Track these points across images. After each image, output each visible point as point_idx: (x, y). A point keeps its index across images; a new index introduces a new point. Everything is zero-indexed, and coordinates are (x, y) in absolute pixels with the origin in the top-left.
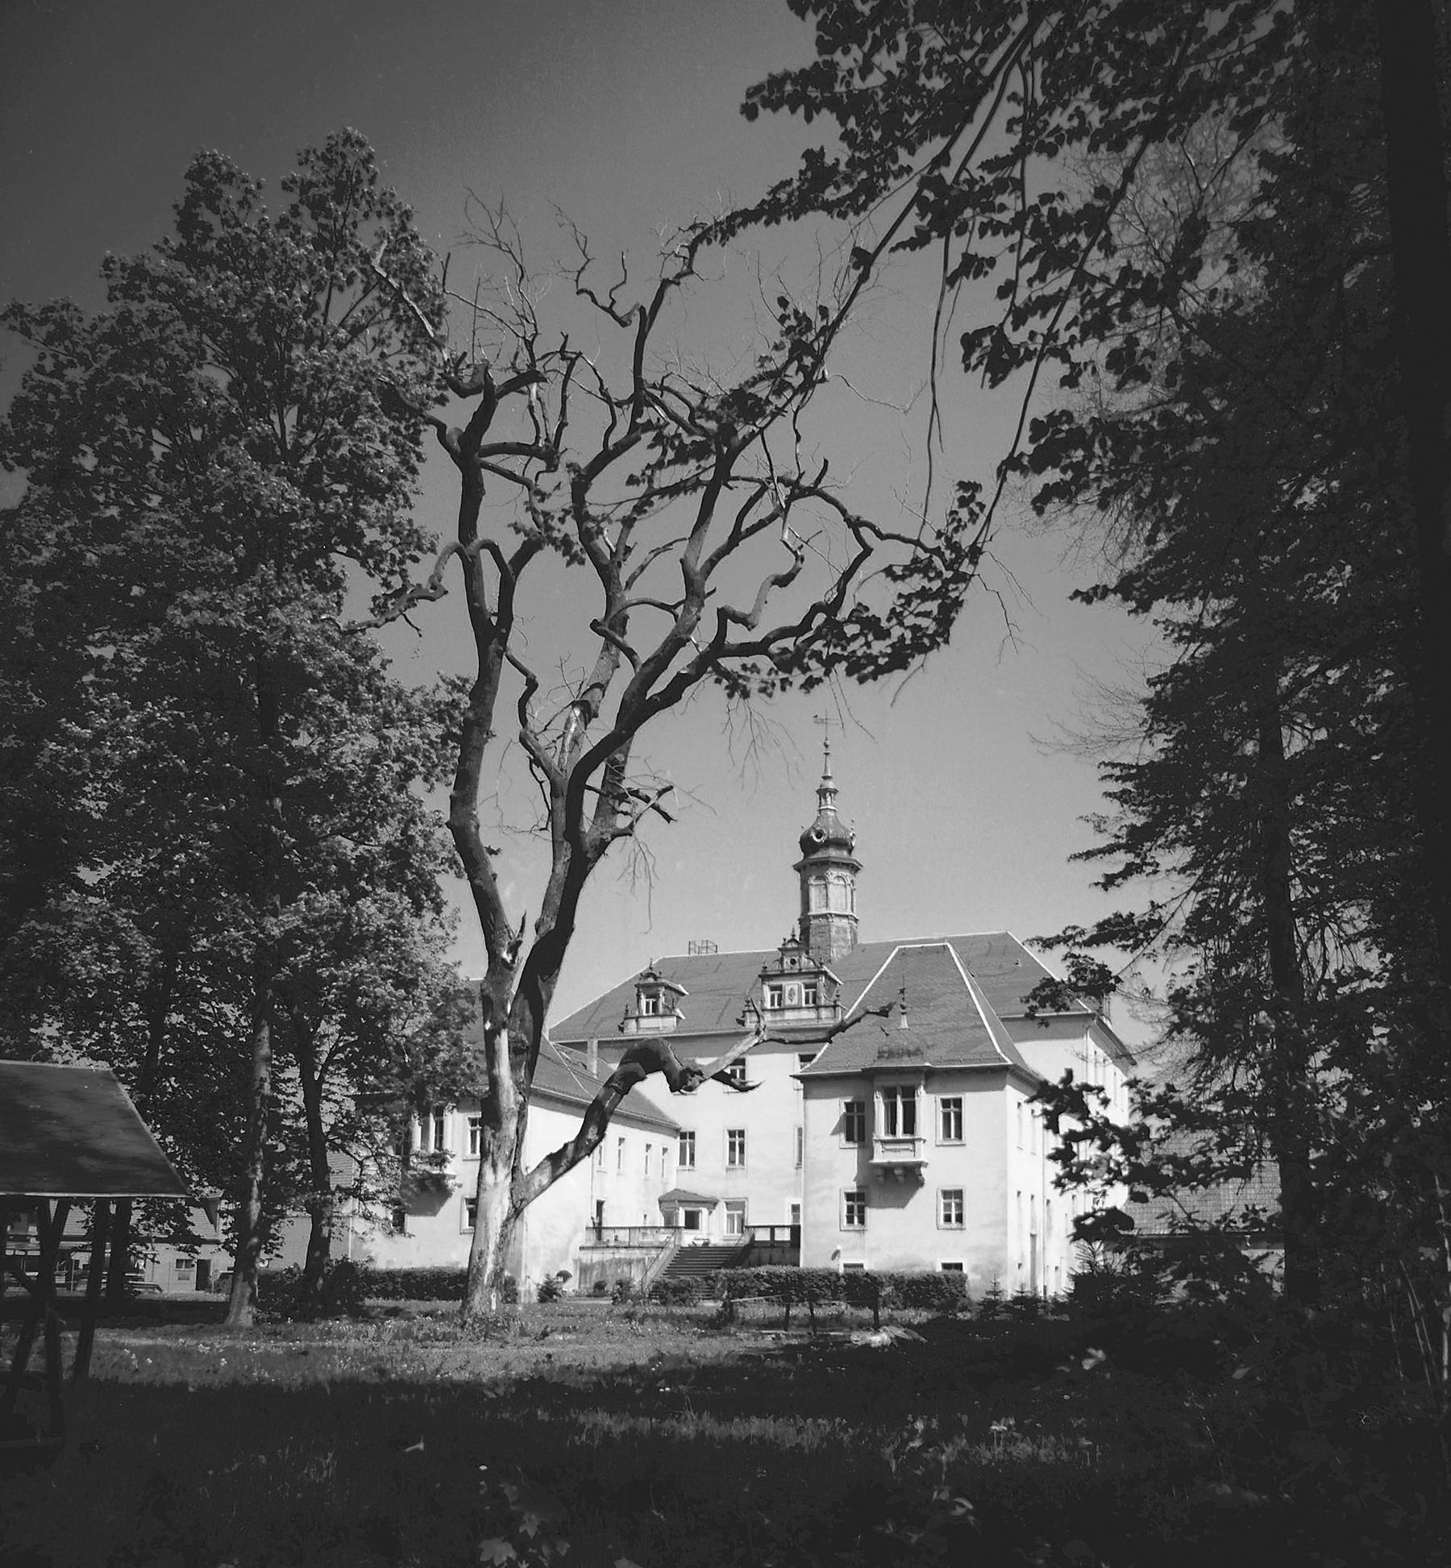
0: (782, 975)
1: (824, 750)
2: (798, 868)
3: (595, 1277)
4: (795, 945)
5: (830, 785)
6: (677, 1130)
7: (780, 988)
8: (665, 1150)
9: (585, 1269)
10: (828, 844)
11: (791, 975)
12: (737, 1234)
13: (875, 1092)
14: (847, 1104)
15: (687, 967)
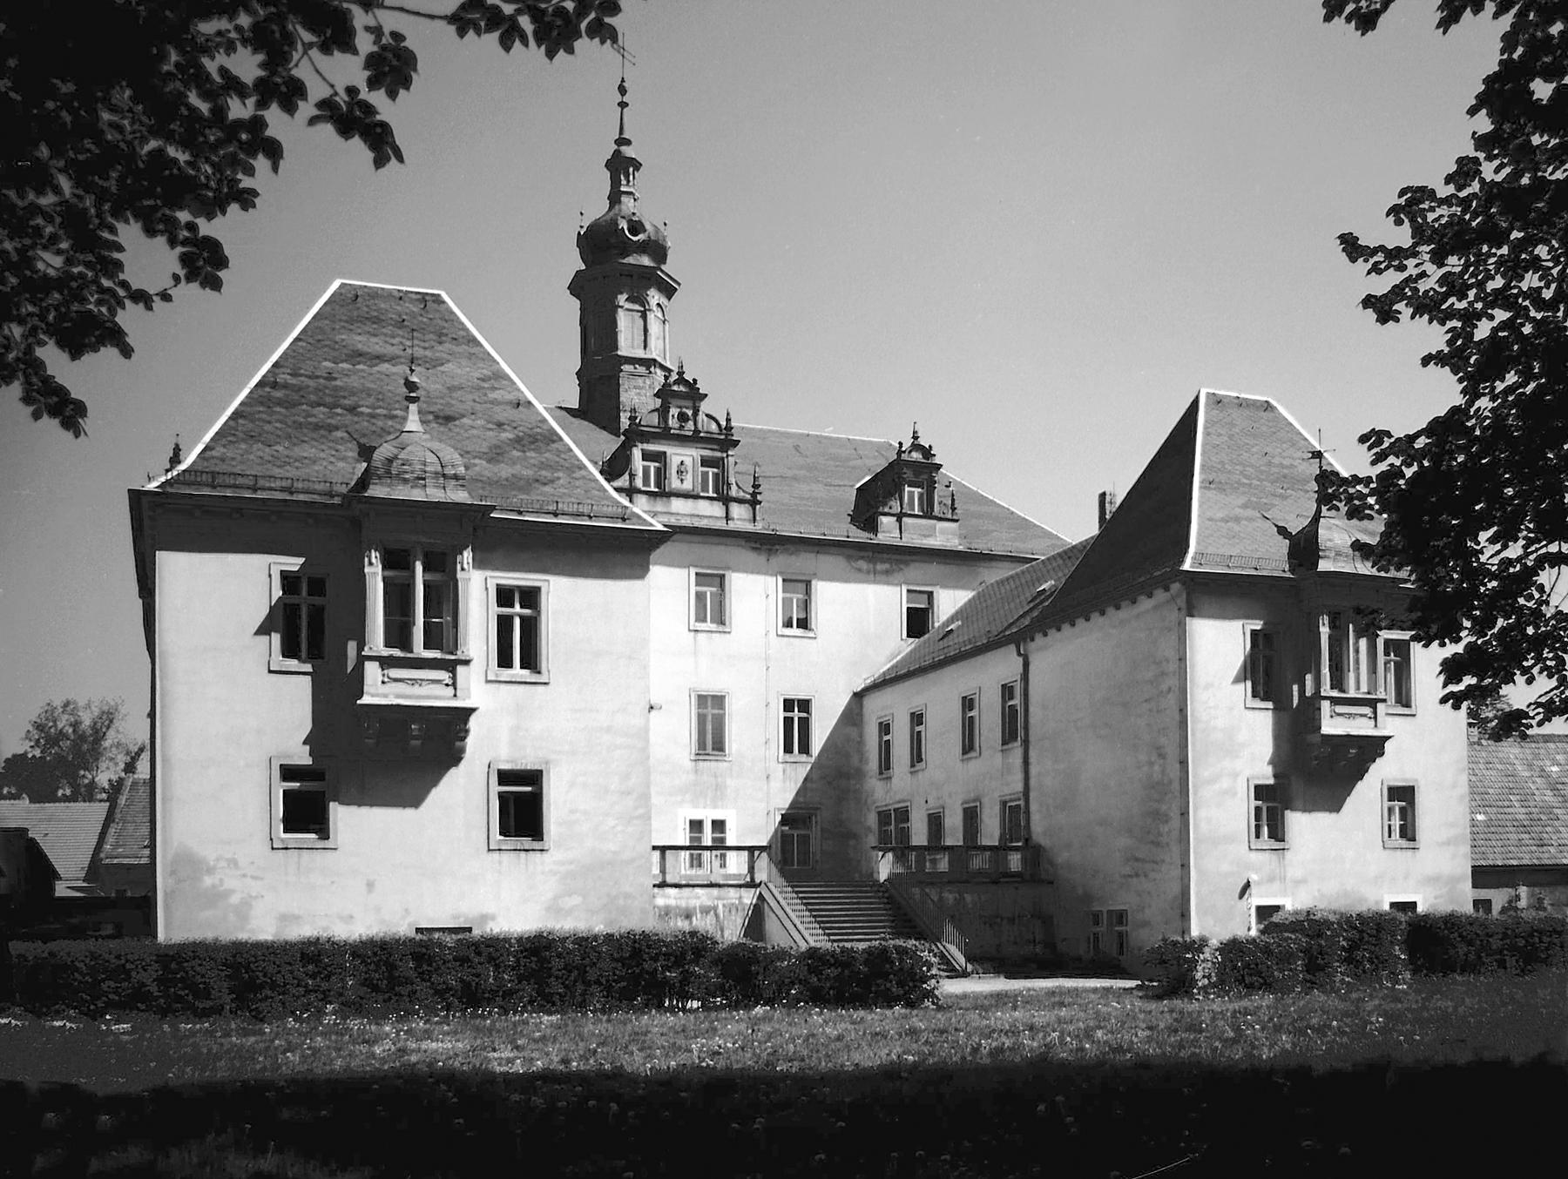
0: (665, 435)
11: (682, 440)
14: (285, 576)
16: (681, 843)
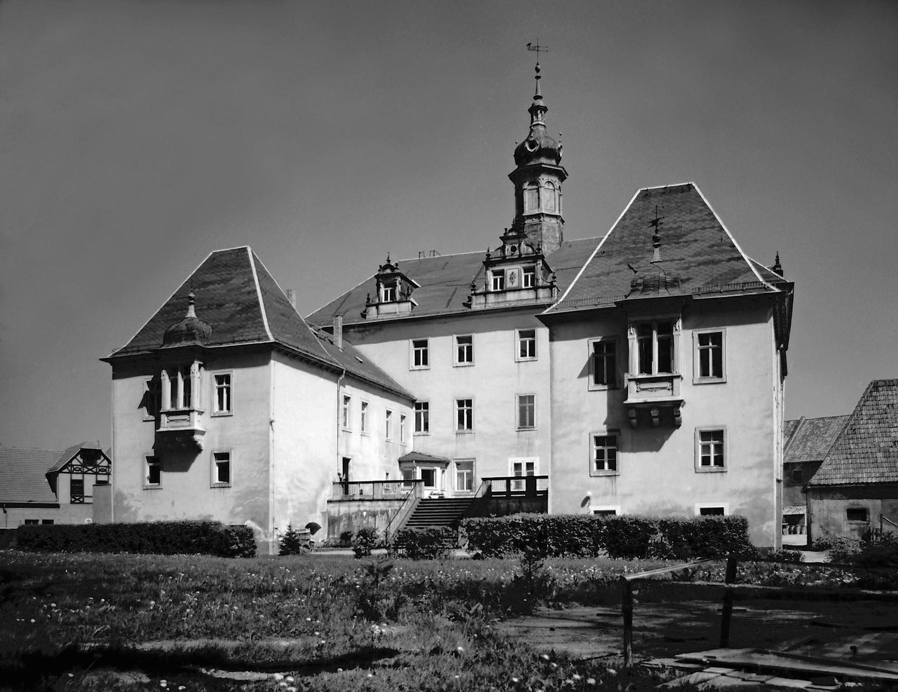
0: (504, 260)
1: (535, 74)
2: (513, 177)
3: (342, 528)
5: (541, 103)
8: (403, 418)
9: (333, 522)
11: (512, 261)
13: (628, 332)
15: (421, 266)
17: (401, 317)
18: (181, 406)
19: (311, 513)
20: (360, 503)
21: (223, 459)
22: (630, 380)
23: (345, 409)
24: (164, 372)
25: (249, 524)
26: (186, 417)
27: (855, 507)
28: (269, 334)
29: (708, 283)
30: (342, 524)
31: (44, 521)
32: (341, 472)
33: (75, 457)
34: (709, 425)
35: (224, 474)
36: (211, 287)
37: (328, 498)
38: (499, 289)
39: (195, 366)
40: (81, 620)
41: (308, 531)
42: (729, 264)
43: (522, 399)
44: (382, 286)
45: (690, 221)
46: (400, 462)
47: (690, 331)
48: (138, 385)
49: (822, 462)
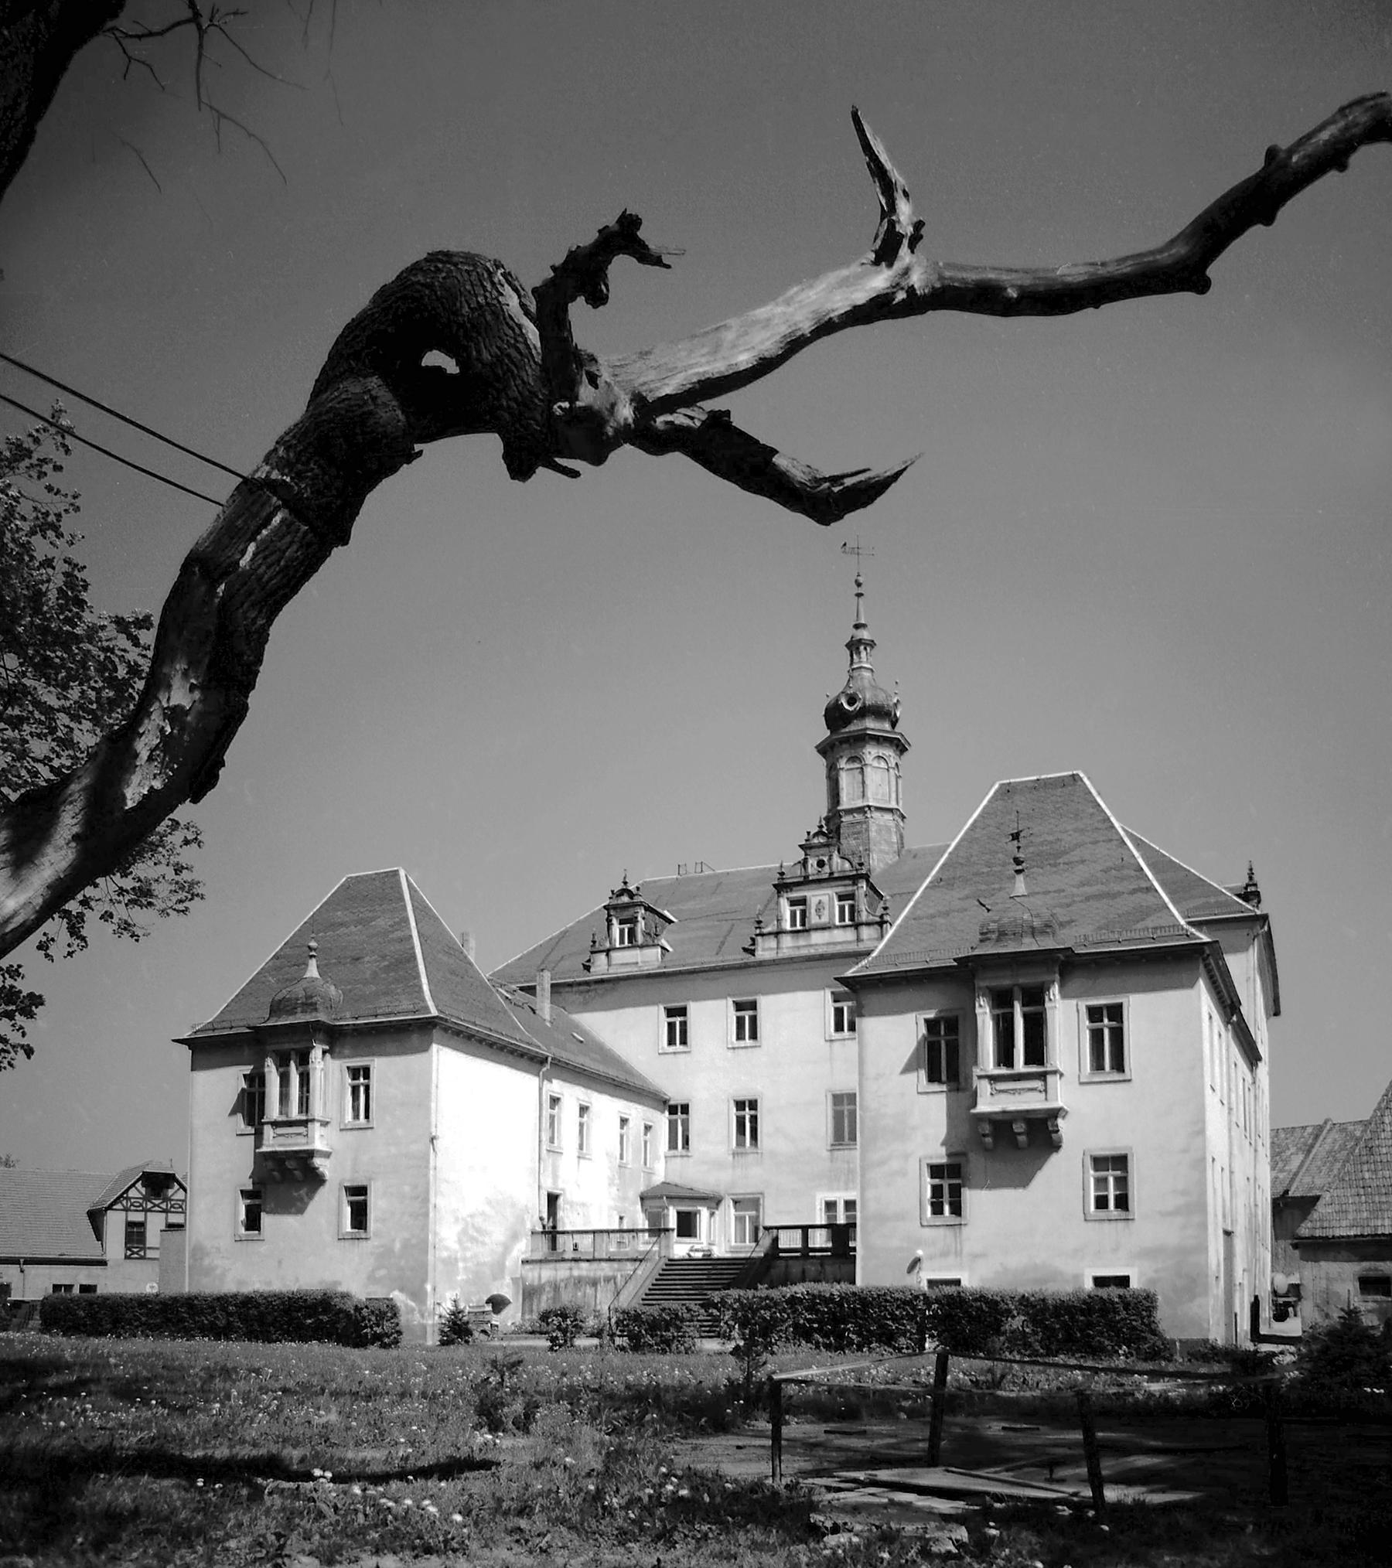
0: (806, 882)
2: (825, 749)
3: (544, 1303)
4: (822, 840)
5: (865, 634)
6: (665, 1102)
7: (803, 901)
8: (648, 1128)
9: (530, 1293)
10: (865, 712)
12: (749, 1244)
13: (979, 998)
14: (927, 1021)
15: (680, 888)
16: (818, 1223)
17: (648, 969)
18: (294, 1113)
19: (495, 1279)
20: (573, 1264)
21: (357, 1192)
22: (980, 1077)
23: (552, 1117)
24: (269, 1062)
25: (399, 1297)
26: (301, 1129)
27: (1372, 1274)
28: (430, 1004)
29: (1100, 928)
30: (544, 1297)
31: (85, 1289)
32: (545, 1215)
33: (133, 1185)
34: (1107, 1147)
35: (360, 1216)
36: (343, 930)
37: (523, 1257)
38: (799, 927)
39: (316, 1053)
40: (123, 1426)
41: (489, 1308)
42: (1133, 898)
43: (838, 1099)
44: (615, 921)
45: (1075, 830)
46: (642, 1199)
47: (1074, 1002)
48: (229, 1081)
49: (1317, 1198)
